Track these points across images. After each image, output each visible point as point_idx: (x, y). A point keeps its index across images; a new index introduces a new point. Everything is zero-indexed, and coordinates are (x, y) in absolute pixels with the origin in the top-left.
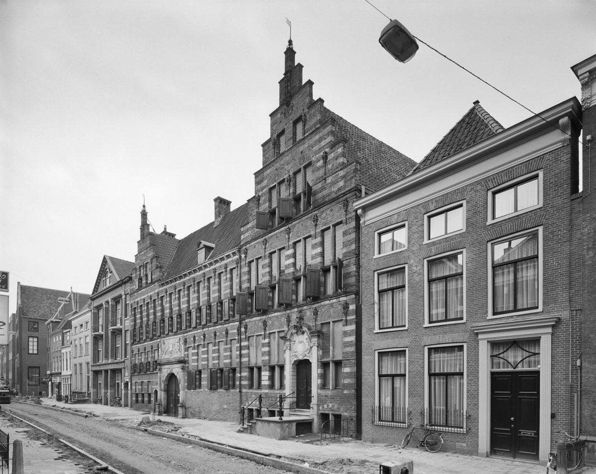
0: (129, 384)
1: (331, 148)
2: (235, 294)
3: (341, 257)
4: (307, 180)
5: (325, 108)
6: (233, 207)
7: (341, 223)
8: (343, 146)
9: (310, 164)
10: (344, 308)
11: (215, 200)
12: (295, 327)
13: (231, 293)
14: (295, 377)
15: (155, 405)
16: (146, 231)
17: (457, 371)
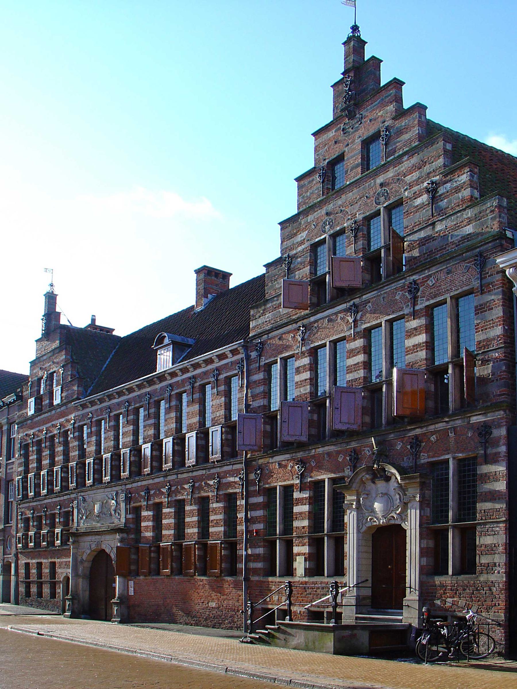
0: (13, 565)
1: (445, 176)
2: (235, 417)
3: (473, 348)
4: (394, 227)
5: (429, 122)
6: (234, 283)
7: (470, 292)
8: (470, 171)
9: (399, 203)
10: (480, 434)
11: (198, 272)
12: (369, 469)
13: (228, 416)
14: (370, 544)
15: (64, 600)
16: (53, 323)
17: (504, 506)
